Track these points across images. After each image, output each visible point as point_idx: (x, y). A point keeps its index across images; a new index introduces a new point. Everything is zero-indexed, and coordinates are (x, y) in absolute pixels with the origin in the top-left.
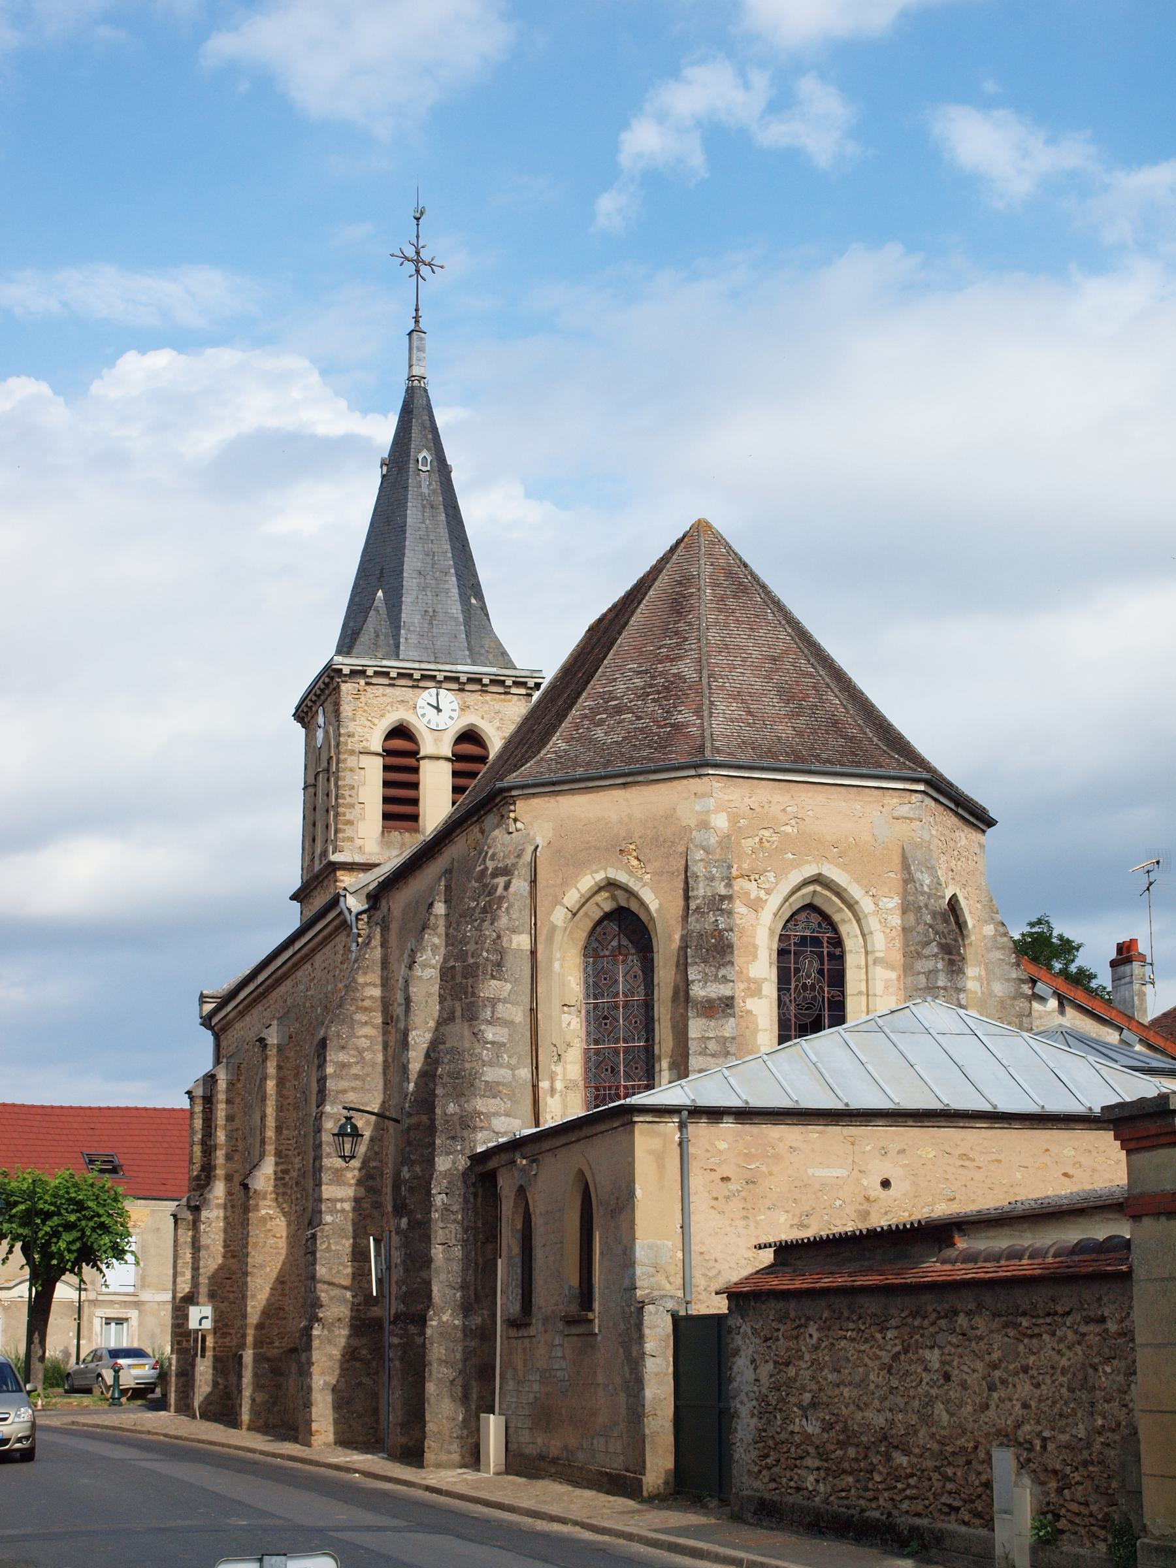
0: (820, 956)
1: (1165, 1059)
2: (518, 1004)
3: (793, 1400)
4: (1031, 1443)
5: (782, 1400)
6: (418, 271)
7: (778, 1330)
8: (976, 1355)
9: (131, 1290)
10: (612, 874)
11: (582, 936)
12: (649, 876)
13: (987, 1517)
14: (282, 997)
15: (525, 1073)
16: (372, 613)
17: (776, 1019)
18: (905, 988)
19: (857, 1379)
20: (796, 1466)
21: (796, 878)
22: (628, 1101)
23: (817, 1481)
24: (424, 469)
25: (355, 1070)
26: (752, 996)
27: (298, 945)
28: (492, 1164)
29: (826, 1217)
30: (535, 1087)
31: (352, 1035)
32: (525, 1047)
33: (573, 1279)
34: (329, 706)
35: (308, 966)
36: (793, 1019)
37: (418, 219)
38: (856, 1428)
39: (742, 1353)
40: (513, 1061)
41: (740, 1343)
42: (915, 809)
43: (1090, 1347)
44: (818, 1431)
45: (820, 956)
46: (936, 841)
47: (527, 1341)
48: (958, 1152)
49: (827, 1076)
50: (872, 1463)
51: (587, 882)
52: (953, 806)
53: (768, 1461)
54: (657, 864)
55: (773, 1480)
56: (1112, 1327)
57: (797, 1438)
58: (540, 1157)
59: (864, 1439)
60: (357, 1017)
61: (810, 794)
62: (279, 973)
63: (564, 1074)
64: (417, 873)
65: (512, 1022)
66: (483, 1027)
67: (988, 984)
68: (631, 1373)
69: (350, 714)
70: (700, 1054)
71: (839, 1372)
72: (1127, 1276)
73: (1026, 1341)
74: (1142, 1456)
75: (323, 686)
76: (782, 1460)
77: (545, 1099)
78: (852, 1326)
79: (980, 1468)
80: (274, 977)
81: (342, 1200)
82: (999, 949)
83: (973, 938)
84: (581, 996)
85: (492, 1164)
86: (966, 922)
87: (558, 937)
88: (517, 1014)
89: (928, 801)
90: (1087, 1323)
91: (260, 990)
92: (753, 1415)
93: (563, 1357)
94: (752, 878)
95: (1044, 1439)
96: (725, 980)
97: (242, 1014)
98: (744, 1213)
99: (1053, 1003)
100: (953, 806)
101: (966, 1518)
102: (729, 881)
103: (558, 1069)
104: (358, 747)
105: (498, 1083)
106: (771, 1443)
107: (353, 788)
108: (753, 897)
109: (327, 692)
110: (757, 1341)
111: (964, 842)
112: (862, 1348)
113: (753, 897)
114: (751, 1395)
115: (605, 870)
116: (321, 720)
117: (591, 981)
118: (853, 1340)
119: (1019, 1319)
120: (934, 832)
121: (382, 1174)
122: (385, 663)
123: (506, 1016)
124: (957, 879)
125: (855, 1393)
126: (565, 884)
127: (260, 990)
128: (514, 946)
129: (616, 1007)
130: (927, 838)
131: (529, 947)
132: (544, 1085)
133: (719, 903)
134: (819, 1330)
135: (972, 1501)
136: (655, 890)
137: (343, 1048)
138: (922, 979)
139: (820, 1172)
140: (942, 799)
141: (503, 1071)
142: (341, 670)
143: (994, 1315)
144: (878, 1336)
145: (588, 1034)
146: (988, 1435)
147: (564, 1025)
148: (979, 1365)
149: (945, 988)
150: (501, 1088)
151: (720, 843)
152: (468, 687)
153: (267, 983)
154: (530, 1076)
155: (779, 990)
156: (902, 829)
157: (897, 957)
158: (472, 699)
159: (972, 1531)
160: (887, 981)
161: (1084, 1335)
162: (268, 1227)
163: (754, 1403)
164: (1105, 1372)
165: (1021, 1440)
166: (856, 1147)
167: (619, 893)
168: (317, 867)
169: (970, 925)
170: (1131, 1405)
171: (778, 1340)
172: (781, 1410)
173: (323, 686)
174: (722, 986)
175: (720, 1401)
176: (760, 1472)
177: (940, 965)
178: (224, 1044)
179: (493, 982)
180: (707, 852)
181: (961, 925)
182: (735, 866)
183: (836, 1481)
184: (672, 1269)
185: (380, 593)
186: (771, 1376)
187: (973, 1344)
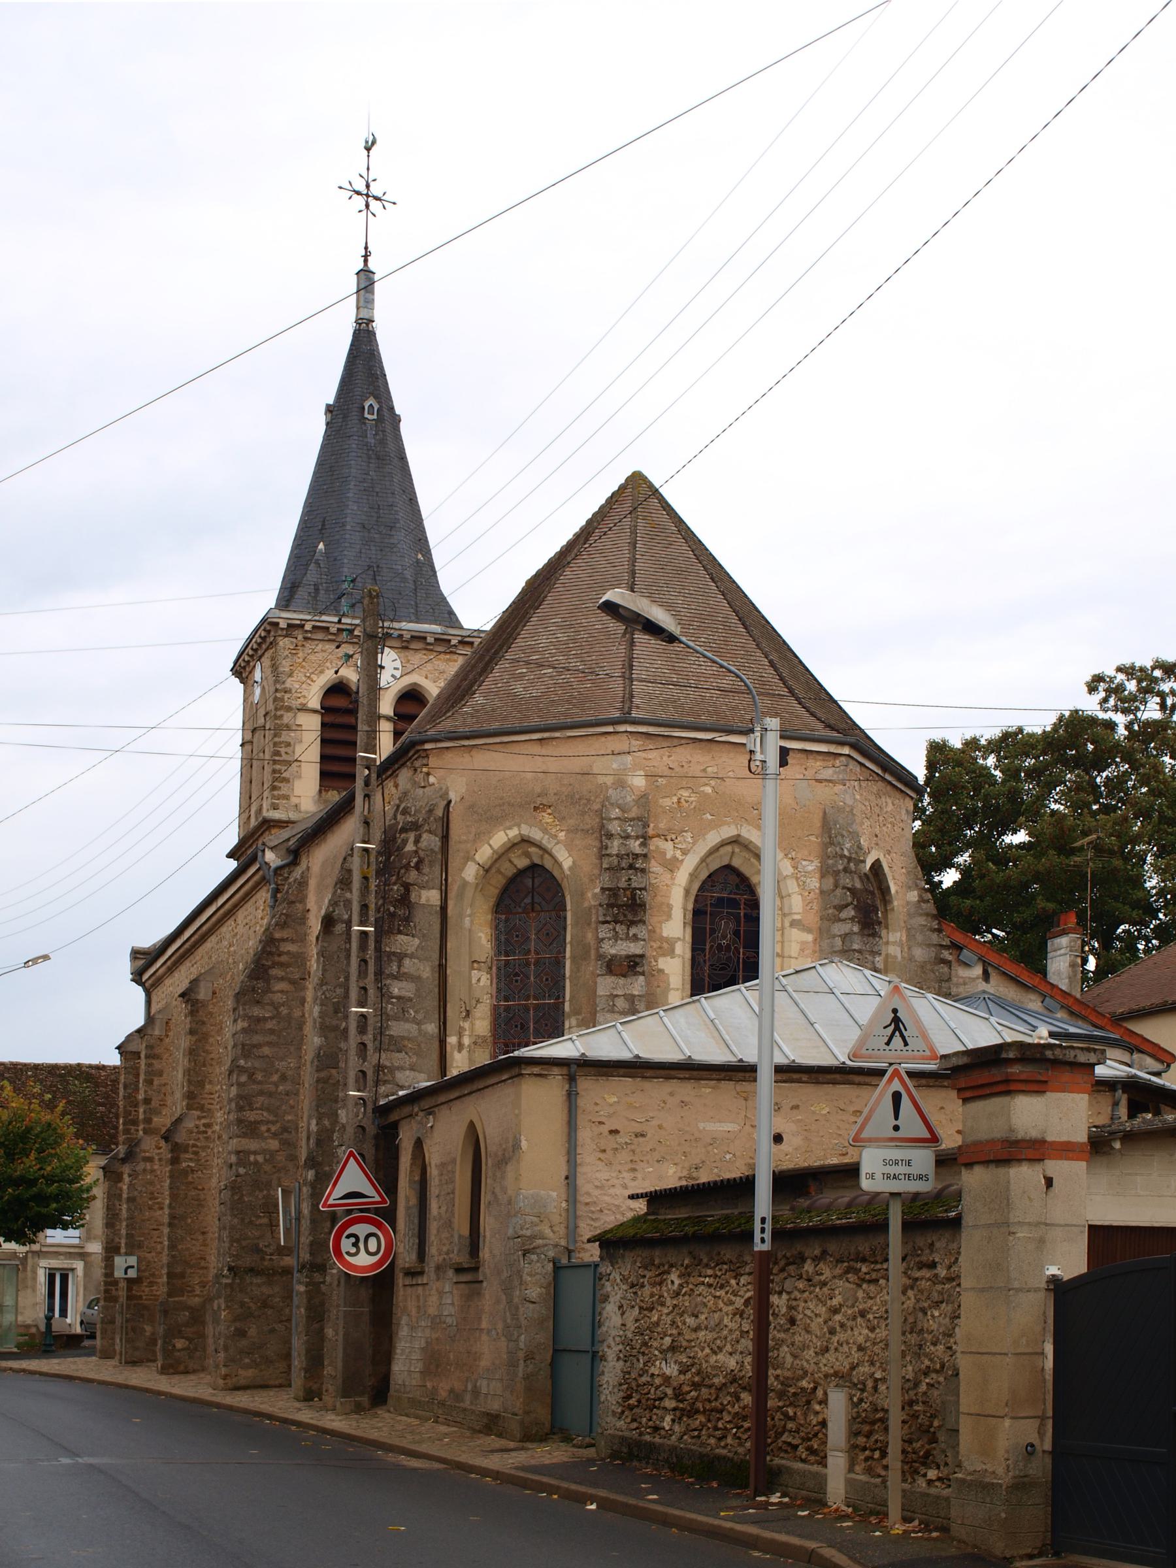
0: (737, 918)
1: (1085, 1026)
2: (427, 959)
3: (655, 1344)
4: (864, 1384)
5: (645, 1344)
6: (367, 206)
7: (644, 1276)
8: (819, 1299)
9: (77, 1241)
10: (526, 830)
11: (494, 892)
12: (563, 833)
13: (822, 1454)
14: (207, 953)
15: (431, 1028)
16: (312, 566)
17: (688, 978)
18: (821, 950)
19: (712, 1323)
20: (655, 1407)
21: (713, 838)
22: (516, 1053)
23: (673, 1421)
24: (370, 417)
25: (270, 1025)
26: (664, 955)
27: (221, 901)
28: (394, 1117)
29: (716, 1170)
30: (442, 1043)
31: (268, 990)
32: (432, 1002)
33: (463, 1227)
34: (266, 660)
35: (231, 922)
36: (707, 979)
37: (368, 149)
38: (709, 1370)
39: (611, 1299)
40: (420, 1017)
41: (609, 1289)
42: (839, 773)
43: (921, 1291)
44: (676, 1373)
45: (737, 918)
46: (860, 805)
47: (420, 1289)
48: (852, 1109)
49: (724, 1032)
50: (722, 1404)
51: (500, 839)
52: (880, 772)
53: (631, 1402)
54: (572, 822)
55: (634, 1420)
56: (942, 1272)
57: (658, 1381)
58: (436, 1110)
59: (716, 1381)
60: (274, 972)
61: (732, 755)
62: (204, 928)
63: (472, 1030)
64: (335, 828)
65: (419, 978)
66: (388, 982)
67: (909, 948)
68: (512, 1319)
69: (287, 669)
70: (608, 1011)
71: (697, 1317)
72: (956, 1223)
73: (865, 1286)
74: (961, 1396)
75: (259, 640)
76: (643, 1401)
77: (452, 1053)
78: (710, 1272)
79: (817, 1407)
80: (200, 932)
81: (255, 1153)
82: (921, 915)
83: (895, 903)
84: (491, 953)
85: (394, 1117)
86: (888, 888)
87: (469, 893)
88: (426, 971)
89: (853, 765)
90: (920, 1269)
91: (187, 946)
92: (619, 1359)
93: (453, 1304)
94: (669, 838)
95: (876, 1380)
96: (635, 938)
97: (170, 971)
98: (630, 1166)
99: (978, 971)
100: (880, 772)
101: (803, 1456)
102: (645, 839)
103: (466, 1025)
104: (295, 704)
105: (403, 1038)
106: (634, 1384)
107: (288, 745)
108: (669, 856)
109: (264, 646)
110: (625, 1287)
111: (890, 808)
112: (718, 1294)
113: (669, 856)
114: (618, 1339)
115: (519, 826)
116: (257, 675)
117: (503, 938)
118: (710, 1286)
119: (859, 1265)
120: (858, 797)
121: (297, 1128)
122: (324, 618)
123: (412, 971)
124: (881, 844)
125: (711, 1336)
126: (481, 837)
127: (187, 946)
128: (423, 901)
129: (528, 964)
130: (850, 802)
131: (439, 903)
132: (452, 1040)
133: (634, 863)
134: (679, 1276)
135: (810, 1439)
136: (569, 847)
137: (258, 1002)
138: (838, 942)
139: (712, 1127)
140: (868, 764)
141: (407, 1026)
142: (278, 624)
143: (837, 1261)
144: (733, 1282)
145: (499, 990)
146: (826, 1376)
147: (474, 981)
148: (822, 1310)
149: (860, 951)
150: (406, 1042)
151: (637, 802)
152: (413, 646)
153: (193, 939)
154: (437, 1031)
155: (693, 950)
156: (825, 793)
157: (813, 919)
158: (417, 658)
159: (807, 1467)
160: (803, 943)
161: (916, 1279)
162: (190, 1179)
163: (621, 1347)
164: (933, 1316)
165: (856, 1381)
166: (750, 1103)
167: (532, 850)
168: (253, 823)
169: (893, 890)
170: (954, 1347)
171: (643, 1286)
172: (643, 1354)
173: (259, 640)
174: (632, 945)
175: (593, 1344)
176: (623, 1412)
177: (856, 929)
178: (154, 998)
179: (401, 937)
180: (623, 811)
181: (884, 891)
182: (652, 825)
183: (690, 1421)
184: (556, 1219)
185: (321, 546)
186: (637, 1321)
187: (817, 1290)
